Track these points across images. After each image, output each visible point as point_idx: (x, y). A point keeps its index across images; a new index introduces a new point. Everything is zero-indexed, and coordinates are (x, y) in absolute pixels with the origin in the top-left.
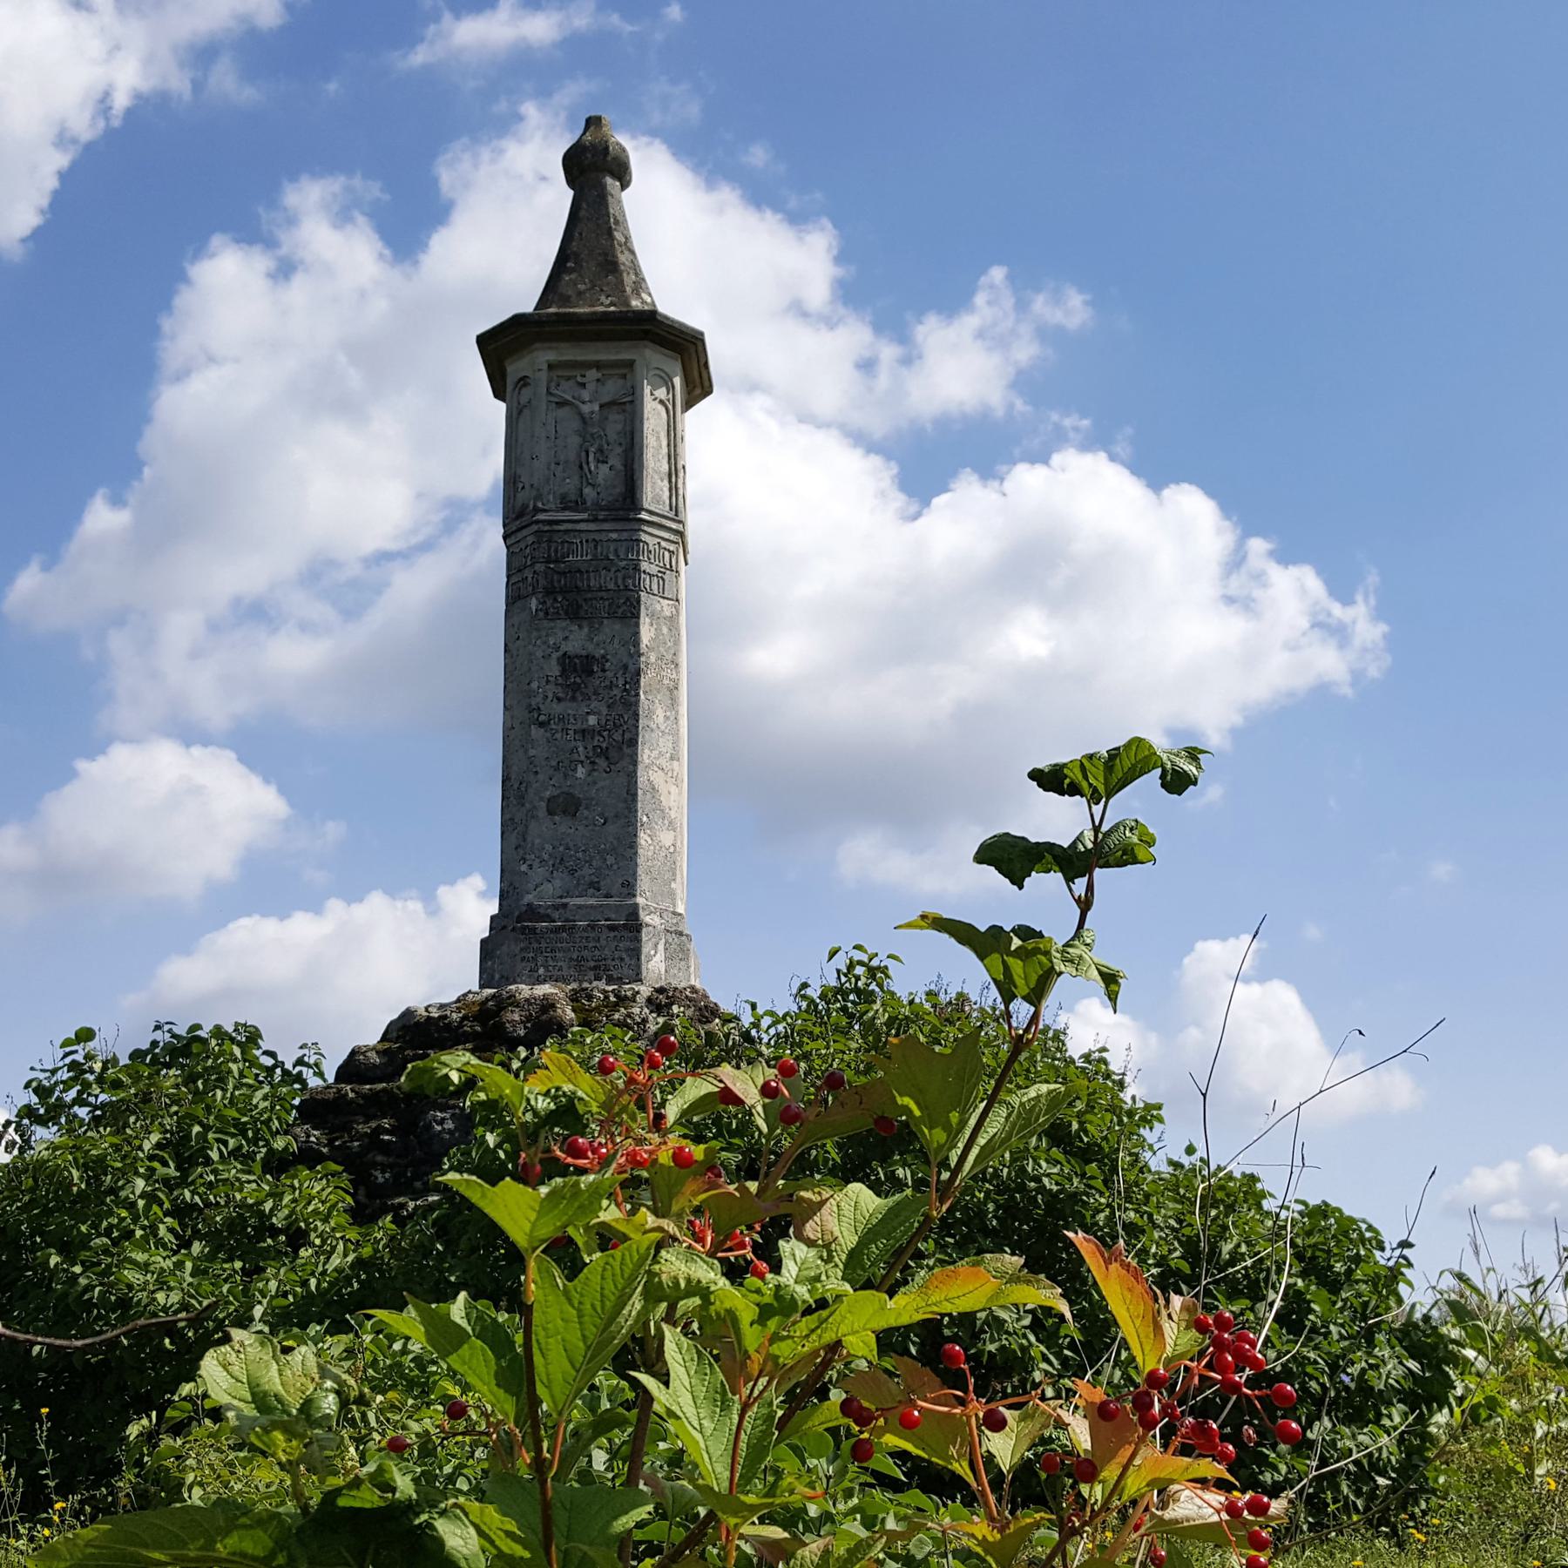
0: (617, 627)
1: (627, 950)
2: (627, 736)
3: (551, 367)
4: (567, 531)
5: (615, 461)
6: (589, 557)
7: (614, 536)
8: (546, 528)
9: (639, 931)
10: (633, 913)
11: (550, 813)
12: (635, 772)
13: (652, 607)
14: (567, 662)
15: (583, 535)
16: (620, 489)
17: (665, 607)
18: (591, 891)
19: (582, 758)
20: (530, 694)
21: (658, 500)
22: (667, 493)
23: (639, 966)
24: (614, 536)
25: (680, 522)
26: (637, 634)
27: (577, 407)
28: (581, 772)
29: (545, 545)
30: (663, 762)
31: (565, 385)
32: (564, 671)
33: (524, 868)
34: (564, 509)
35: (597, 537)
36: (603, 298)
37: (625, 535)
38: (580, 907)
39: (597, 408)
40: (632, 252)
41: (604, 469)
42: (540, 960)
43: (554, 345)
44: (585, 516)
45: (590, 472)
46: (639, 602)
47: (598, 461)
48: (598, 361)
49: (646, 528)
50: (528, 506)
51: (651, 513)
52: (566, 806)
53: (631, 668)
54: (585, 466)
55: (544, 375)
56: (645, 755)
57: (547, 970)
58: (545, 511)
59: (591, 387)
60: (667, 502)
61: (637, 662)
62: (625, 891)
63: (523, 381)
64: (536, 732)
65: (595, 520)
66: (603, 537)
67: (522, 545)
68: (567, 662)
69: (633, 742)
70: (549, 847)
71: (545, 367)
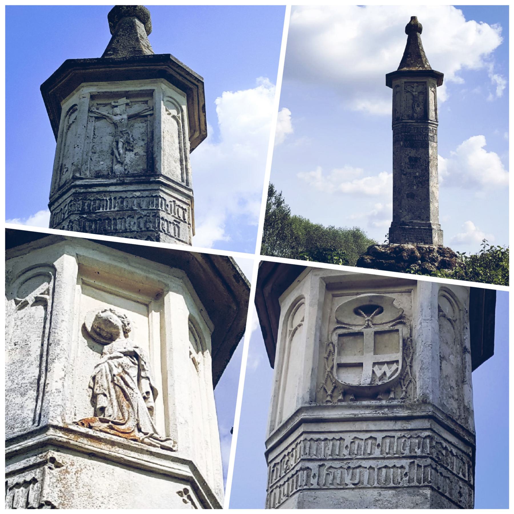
0: (423, 150)
1: (429, 235)
2: (427, 178)
3: (93, 97)
4: (98, 193)
5: (140, 149)
6: (116, 209)
7: (138, 194)
8: (82, 191)
9: (432, 231)
10: (430, 225)
11: (407, 197)
12: (429, 188)
13: (432, 144)
14: (410, 158)
15: (112, 194)
16: (142, 166)
17: (434, 144)
18: (418, 219)
19: (415, 183)
20: (402, 166)
21: (432, 117)
22: (434, 115)
23: (432, 240)
24: (138, 194)
25: (190, 190)
26: (428, 152)
27: (111, 119)
28: (415, 187)
29: (80, 202)
30: (435, 185)
31: (408, 87)
32: (410, 161)
33: (401, 211)
34: (409, 119)
35: (123, 195)
36: (418, 65)
37: (146, 193)
38: (416, 223)
39: (417, 93)
40: (424, 52)
41: (419, 108)
42: (407, 236)
43: (95, 83)
44: (414, 121)
45: (119, 154)
46: (428, 143)
47: (126, 150)
48: (127, 92)
49: (163, 189)
50: (399, 118)
51: (431, 121)
52: (411, 196)
53: (427, 161)
54: (116, 151)
55: (403, 85)
56: (431, 183)
57: (408, 239)
58: (82, 179)
59: (415, 88)
60: (180, 177)
61: (428, 160)
62: (427, 219)
63: (398, 86)
64: (403, 176)
65: (417, 122)
66: (129, 195)
67: (62, 207)
68: (410, 158)
69: (428, 180)
70: (407, 206)
71: (404, 83)
